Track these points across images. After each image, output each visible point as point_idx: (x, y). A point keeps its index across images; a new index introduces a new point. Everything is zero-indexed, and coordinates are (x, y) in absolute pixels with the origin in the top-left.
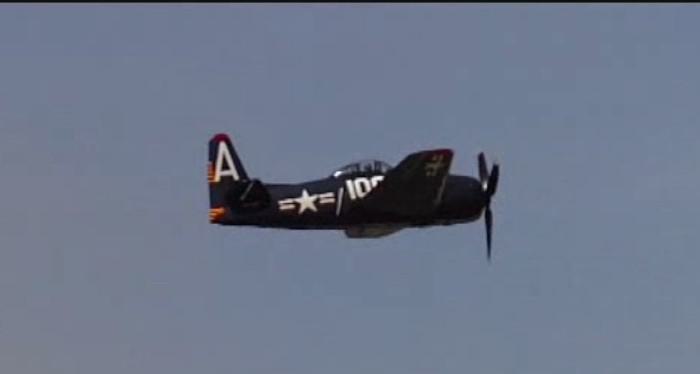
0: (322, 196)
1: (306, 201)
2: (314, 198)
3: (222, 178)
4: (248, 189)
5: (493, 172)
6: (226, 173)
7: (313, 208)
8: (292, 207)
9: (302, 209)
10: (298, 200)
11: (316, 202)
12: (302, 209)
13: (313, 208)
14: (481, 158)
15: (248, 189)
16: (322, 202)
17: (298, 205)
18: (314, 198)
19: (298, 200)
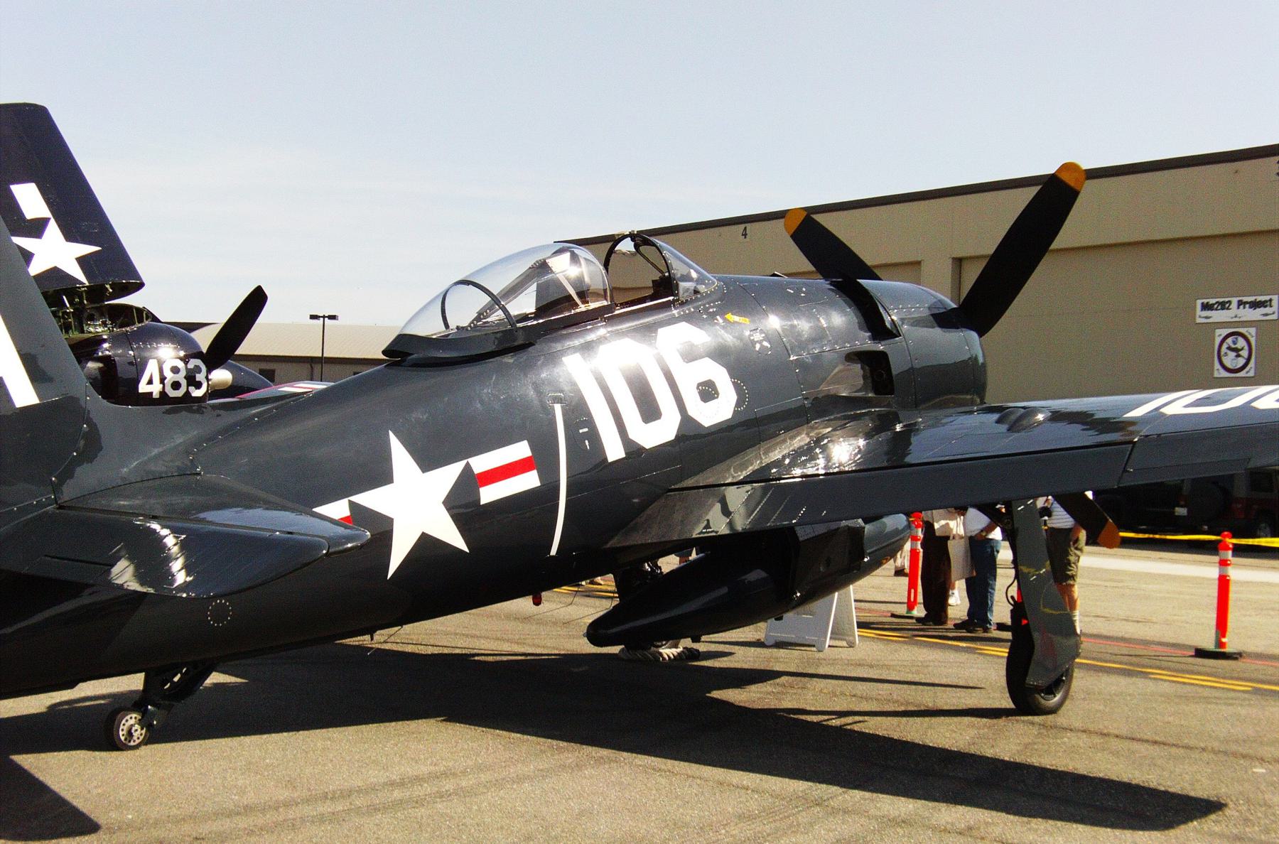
0: (481, 463)
2: (448, 475)
10: (371, 499)
11: (462, 505)
13: (453, 537)
16: (489, 494)
18: (448, 475)
19: (371, 499)
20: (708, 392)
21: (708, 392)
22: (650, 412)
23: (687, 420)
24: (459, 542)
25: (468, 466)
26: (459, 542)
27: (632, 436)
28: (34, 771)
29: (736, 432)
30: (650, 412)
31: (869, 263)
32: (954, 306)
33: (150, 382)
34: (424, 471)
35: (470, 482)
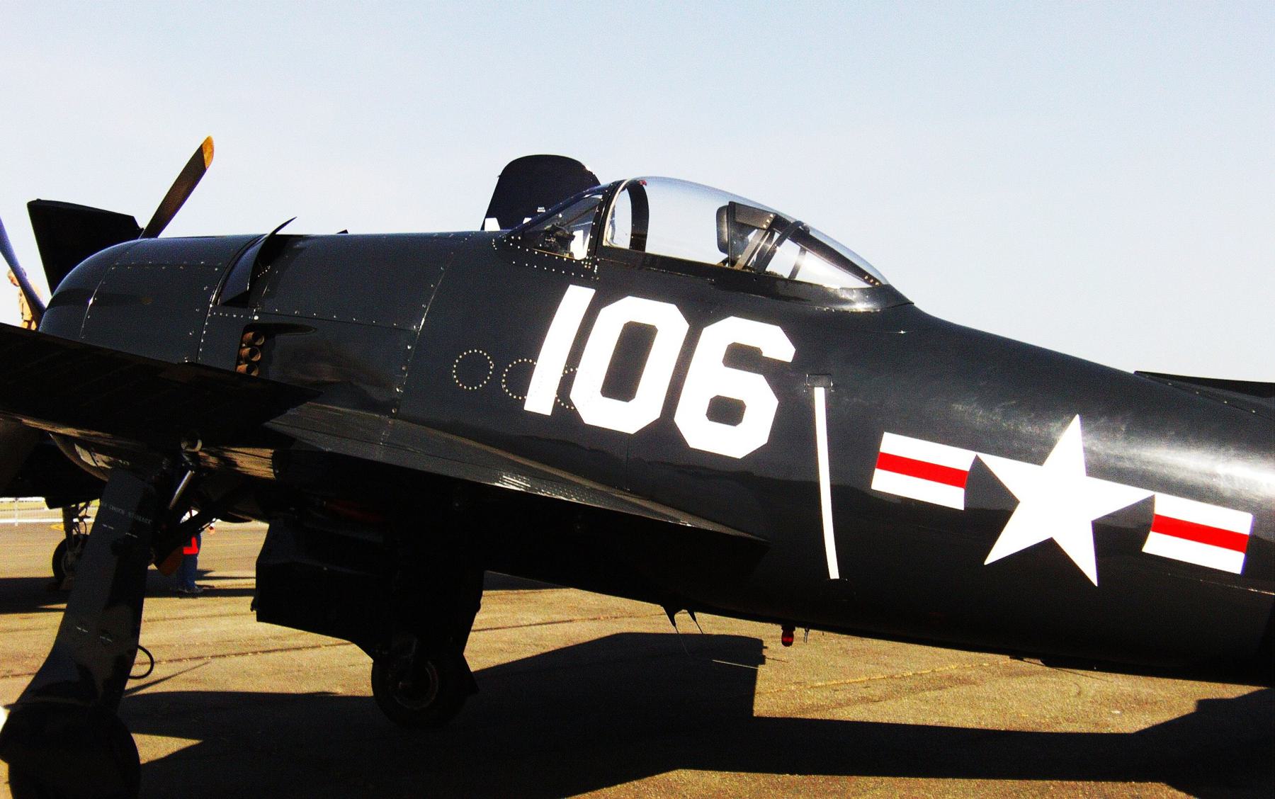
7: (1085, 559)
11: (1117, 536)
16: (1158, 545)
17: (992, 507)
19: (1004, 469)
20: (726, 411)
21: (726, 411)
22: (621, 383)
25: (1150, 502)
27: (576, 396)
30: (621, 383)
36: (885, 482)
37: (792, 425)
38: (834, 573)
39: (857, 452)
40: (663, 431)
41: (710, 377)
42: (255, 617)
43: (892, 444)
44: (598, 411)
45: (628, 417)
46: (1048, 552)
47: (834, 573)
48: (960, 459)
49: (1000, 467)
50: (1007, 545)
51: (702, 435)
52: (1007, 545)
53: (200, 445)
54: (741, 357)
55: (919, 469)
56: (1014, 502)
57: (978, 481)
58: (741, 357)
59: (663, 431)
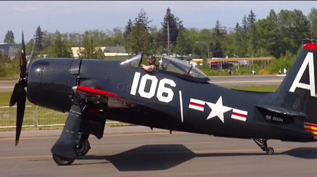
0: (235, 110)
1: (218, 110)
2: (228, 109)
3: (297, 89)
4: (168, 30)
5: (106, 159)
6: (304, 86)
7: (222, 118)
8: (202, 109)
9: (211, 116)
10: (210, 104)
11: (227, 115)
12: (211, 116)
13: (222, 118)
14: (218, 22)
15: (168, 30)
16: (233, 117)
17: (208, 110)
18: (228, 109)
19: (210, 104)
20: (165, 95)
21: (165, 95)
22: (147, 89)
23: (155, 97)
24: (223, 122)
25: (232, 110)
26: (223, 122)
27: (139, 92)
28: (213, 117)
29: (72, 76)
30: (147, 89)
31: (111, 165)
32: (282, 81)
33: (305, 79)
34: (215, 103)
35: (231, 112)
36: (191, 106)
37: (176, 97)
38: (180, 92)
39: (187, 103)
40: (155, 97)
41: (162, 89)
42: (284, 9)
43: (192, 100)
44: (143, 94)
45: (149, 95)
46: (217, 117)
47: (180, 92)
48: (203, 103)
49: (209, 104)
50: (210, 117)
51: (161, 98)
52: (210, 117)
53: (227, 57)
54: (167, 86)
55: (197, 105)
56: (211, 110)
57: (206, 107)
58: (167, 86)
59: (155, 97)
